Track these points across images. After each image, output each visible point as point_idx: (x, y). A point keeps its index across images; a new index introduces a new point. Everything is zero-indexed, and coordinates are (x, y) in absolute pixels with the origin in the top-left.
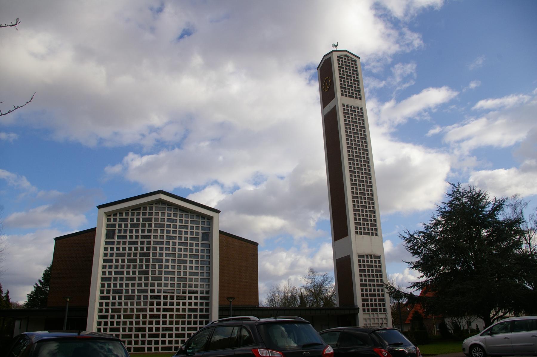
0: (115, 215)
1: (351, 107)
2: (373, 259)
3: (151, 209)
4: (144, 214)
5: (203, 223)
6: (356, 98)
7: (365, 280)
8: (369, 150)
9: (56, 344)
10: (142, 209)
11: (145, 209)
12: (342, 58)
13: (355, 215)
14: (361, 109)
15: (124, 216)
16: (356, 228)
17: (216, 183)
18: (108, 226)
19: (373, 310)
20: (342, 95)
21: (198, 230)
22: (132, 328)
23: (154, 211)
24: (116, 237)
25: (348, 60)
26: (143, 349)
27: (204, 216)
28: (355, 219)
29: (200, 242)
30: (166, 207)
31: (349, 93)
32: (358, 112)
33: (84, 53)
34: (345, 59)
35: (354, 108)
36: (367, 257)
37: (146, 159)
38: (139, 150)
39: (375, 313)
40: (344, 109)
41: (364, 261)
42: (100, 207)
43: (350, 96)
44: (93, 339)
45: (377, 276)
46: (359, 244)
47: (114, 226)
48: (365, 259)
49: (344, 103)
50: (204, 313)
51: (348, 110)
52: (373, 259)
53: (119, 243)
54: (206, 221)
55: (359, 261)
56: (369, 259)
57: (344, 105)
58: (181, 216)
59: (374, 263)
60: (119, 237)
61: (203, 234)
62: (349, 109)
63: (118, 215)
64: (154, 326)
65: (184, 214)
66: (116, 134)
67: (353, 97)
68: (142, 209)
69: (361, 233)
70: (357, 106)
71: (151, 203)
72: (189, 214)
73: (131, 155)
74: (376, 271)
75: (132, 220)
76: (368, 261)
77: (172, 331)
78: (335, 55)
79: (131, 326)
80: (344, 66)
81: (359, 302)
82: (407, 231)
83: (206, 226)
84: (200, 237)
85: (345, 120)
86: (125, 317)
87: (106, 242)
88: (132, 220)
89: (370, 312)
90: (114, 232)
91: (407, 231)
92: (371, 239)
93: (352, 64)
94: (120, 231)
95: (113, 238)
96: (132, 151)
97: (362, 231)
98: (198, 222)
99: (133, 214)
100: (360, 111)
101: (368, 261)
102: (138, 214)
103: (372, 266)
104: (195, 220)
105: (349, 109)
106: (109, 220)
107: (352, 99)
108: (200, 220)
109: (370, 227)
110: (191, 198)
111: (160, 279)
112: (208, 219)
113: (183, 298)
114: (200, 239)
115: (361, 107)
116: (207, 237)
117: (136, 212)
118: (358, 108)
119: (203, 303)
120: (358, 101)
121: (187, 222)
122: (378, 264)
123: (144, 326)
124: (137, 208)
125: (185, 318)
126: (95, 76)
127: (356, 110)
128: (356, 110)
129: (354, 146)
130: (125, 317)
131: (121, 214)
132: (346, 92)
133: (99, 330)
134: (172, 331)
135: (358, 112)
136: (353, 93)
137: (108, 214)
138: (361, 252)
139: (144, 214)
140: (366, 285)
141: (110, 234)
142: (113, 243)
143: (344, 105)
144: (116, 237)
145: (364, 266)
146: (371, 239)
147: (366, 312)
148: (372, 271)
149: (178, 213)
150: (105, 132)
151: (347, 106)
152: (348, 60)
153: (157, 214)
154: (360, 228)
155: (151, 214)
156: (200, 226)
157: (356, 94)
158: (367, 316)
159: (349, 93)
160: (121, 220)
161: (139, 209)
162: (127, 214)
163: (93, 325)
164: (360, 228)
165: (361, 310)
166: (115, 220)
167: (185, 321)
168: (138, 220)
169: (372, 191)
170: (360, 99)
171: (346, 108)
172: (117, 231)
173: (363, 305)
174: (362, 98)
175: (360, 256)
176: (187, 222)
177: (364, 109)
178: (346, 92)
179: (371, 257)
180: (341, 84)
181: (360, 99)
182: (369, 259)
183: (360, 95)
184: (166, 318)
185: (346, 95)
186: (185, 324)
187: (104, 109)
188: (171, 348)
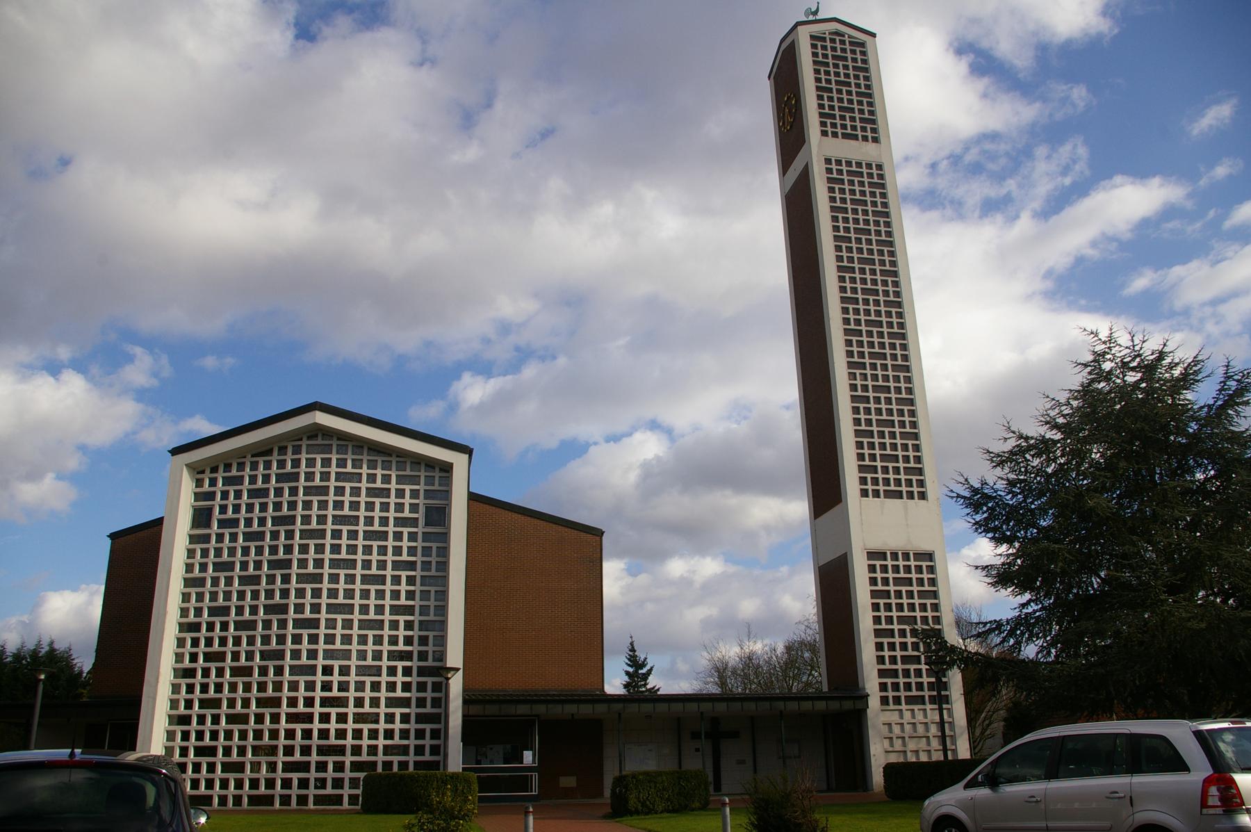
0: (214, 470)
1: (849, 163)
2: (912, 563)
3: (297, 450)
4: (282, 464)
5: (429, 481)
6: (865, 139)
7: (893, 660)
8: (901, 273)
9: (88, 774)
10: (276, 452)
11: (283, 450)
12: (824, 39)
13: (860, 445)
14: (880, 167)
15: (234, 472)
16: (863, 481)
17: (654, 426)
18: (198, 496)
19: (911, 700)
20: (824, 133)
21: (407, 498)
22: (395, 683)
23: (304, 457)
24: (215, 525)
25: (843, 42)
26: (269, 800)
27: (431, 463)
28: (861, 457)
29: (420, 530)
30: (335, 443)
31: (844, 127)
32: (870, 175)
33: (337, 197)
34: (833, 41)
35: (859, 165)
36: (895, 556)
37: (494, 384)
38: (484, 369)
39: (916, 707)
40: (829, 171)
41: (884, 569)
42: (176, 451)
43: (845, 136)
44: (147, 769)
45: (923, 607)
46: (873, 523)
47: (211, 496)
48: (889, 563)
49: (829, 154)
50: (428, 709)
51: (840, 172)
52: (912, 563)
53: (220, 538)
54: (437, 474)
55: (872, 569)
56: (901, 563)
57: (828, 161)
58: (372, 465)
59: (914, 572)
60: (222, 524)
61: (429, 509)
62: (844, 168)
63: (221, 469)
64: (333, 726)
65: (380, 459)
66: (428, 344)
67: (855, 137)
68: (276, 452)
69: (876, 494)
70: (864, 159)
71: (296, 435)
72: (394, 460)
73: (467, 377)
74: (922, 594)
75: (253, 479)
76: (896, 569)
77: (344, 754)
78: (804, 35)
79: (359, 694)
80: (833, 86)
81: (871, 682)
82: (962, 480)
83: (436, 487)
84: (420, 515)
85: (836, 229)
86: (362, 671)
87: (191, 536)
88: (253, 479)
89: (904, 706)
90: (210, 510)
91: (962, 480)
92: (906, 509)
93: (853, 52)
94: (223, 509)
95: (209, 526)
96: (469, 369)
97: (881, 488)
98: (414, 480)
99: (254, 466)
100: (875, 171)
101: (896, 569)
102: (268, 465)
103: (909, 582)
104: (408, 472)
105: (844, 168)
106: (199, 483)
107: (853, 142)
108: (423, 474)
109: (901, 476)
110: (416, 418)
111: (314, 624)
112: (441, 470)
113: (374, 671)
114: (421, 522)
115: (879, 161)
116: (438, 516)
117: (261, 460)
118: (869, 166)
119: (425, 683)
120: (870, 146)
121: (386, 479)
122: (925, 576)
123: (274, 742)
124: (263, 451)
125: (377, 722)
126: (375, 240)
127: (864, 170)
128: (864, 170)
129: (849, 206)
130: (362, 671)
131: (228, 467)
132: (834, 125)
133: (170, 751)
134: (344, 754)
135: (870, 175)
136: (854, 128)
137: (197, 470)
138: (876, 545)
139: (282, 464)
140: (894, 673)
141: (201, 517)
142: (207, 539)
143: (828, 161)
144: (215, 525)
145: (886, 581)
146: (906, 509)
147: (892, 706)
148: (910, 594)
149: (365, 458)
150: (407, 341)
151: (839, 162)
152: (843, 42)
153: (311, 462)
154: (875, 481)
155: (296, 463)
156: (421, 487)
157: (864, 129)
158: (894, 717)
159: (844, 127)
160: (227, 481)
161: (269, 452)
162: (241, 467)
163: (156, 738)
164: (875, 481)
165: (874, 702)
166: (213, 482)
167: (376, 731)
168: (266, 479)
169: (908, 380)
170: (876, 140)
171: (834, 167)
172: (217, 510)
173: (883, 687)
174: (882, 139)
175: (872, 555)
176: (386, 479)
177: (886, 167)
178: (834, 125)
179: (906, 556)
180: (821, 106)
181: (876, 140)
182: (901, 563)
183: (874, 130)
184: (328, 722)
185: (835, 135)
186: (376, 738)
187: (394, 295)
188: (338, 800)
